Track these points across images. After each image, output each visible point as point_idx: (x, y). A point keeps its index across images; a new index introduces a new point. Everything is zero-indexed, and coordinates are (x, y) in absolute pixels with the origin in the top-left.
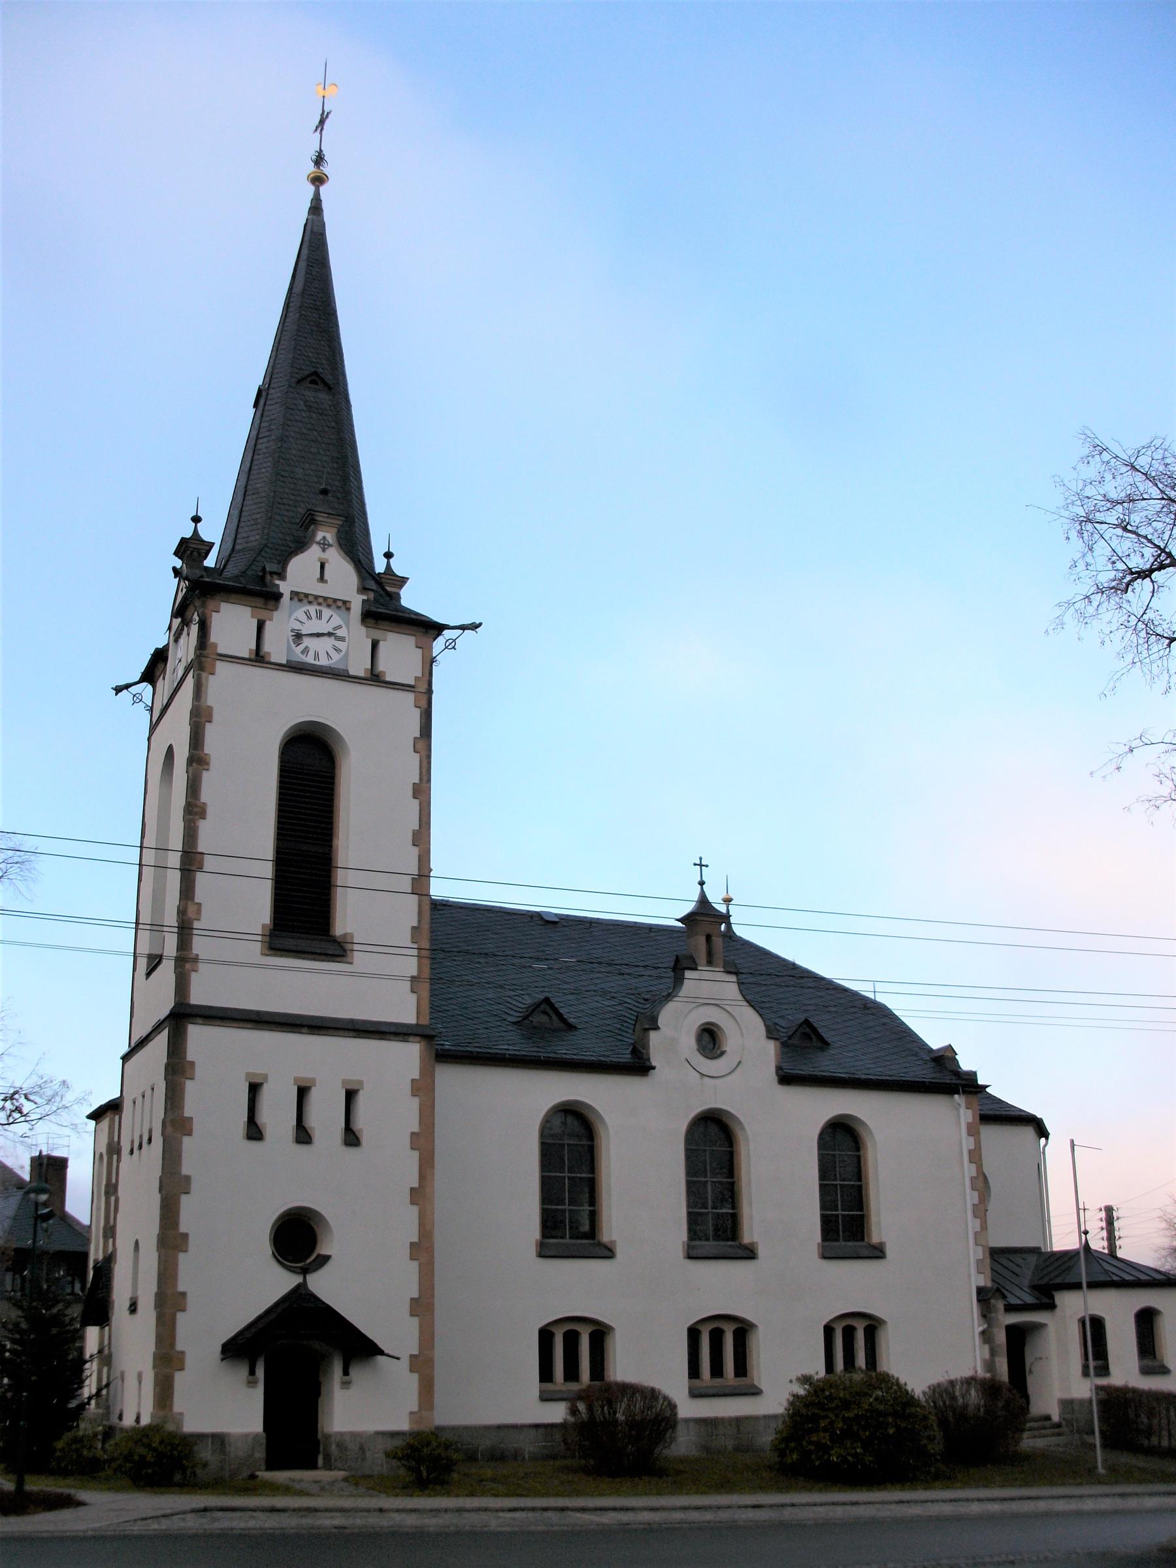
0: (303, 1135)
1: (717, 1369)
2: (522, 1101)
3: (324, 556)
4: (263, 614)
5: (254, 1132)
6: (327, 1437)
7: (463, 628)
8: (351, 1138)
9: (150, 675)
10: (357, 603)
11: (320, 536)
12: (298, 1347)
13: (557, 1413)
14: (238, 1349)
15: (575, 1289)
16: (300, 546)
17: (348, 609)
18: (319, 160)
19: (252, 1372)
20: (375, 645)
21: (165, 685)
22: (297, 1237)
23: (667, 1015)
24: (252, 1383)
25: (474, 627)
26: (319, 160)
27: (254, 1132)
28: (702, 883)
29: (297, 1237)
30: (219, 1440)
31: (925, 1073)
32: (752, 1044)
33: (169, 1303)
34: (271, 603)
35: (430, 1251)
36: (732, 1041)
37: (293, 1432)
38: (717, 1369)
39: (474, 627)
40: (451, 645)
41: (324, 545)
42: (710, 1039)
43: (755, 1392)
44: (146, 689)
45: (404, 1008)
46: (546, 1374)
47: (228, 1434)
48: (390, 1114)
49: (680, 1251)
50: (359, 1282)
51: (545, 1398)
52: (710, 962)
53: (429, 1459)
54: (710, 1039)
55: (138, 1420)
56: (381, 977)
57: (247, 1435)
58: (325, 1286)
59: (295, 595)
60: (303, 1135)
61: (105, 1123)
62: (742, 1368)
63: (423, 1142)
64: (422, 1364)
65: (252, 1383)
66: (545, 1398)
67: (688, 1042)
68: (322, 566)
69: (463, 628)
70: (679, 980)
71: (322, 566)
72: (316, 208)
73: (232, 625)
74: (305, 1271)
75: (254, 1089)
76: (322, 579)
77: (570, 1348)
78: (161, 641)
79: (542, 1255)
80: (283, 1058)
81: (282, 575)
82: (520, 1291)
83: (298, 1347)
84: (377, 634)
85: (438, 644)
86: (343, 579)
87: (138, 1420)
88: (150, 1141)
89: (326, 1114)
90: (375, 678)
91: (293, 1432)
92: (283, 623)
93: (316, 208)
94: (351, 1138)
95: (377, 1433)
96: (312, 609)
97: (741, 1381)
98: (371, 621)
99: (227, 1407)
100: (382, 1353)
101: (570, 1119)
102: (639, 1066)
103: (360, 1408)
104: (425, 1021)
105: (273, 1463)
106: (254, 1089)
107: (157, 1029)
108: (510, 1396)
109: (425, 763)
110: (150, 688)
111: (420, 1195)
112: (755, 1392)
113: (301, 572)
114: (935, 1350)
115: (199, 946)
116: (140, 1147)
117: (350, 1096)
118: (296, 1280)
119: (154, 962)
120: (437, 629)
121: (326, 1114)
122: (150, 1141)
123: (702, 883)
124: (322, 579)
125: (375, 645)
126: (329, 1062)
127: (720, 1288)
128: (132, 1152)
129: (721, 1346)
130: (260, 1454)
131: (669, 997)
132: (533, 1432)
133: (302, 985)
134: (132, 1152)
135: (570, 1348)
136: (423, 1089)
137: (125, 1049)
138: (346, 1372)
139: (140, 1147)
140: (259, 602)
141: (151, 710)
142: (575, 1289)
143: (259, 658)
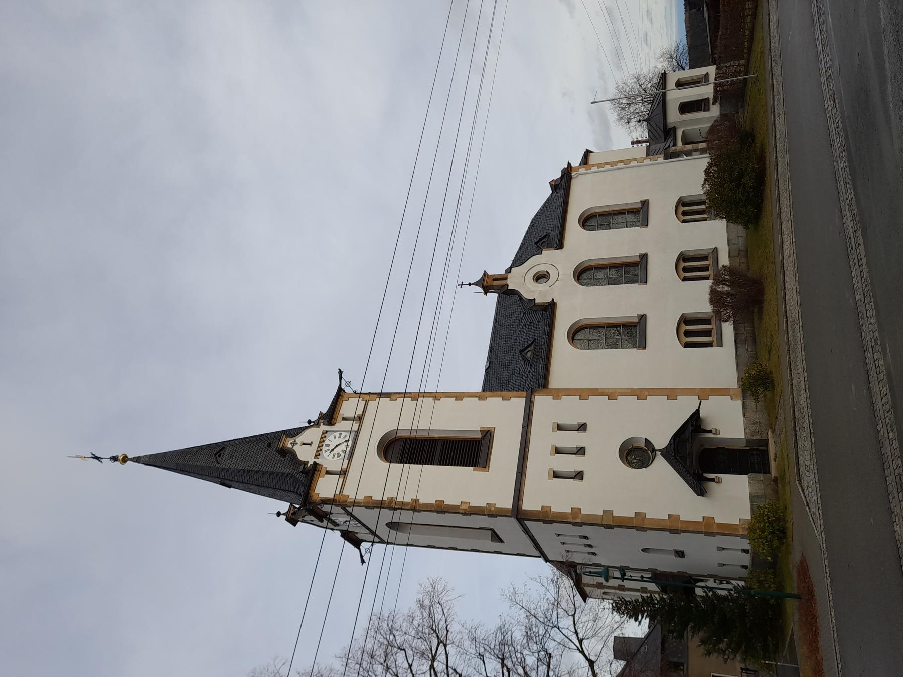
0: (581, 451)
1: (708, 333)
2: (568, 362)
3: (299, 444)
4: (323, 472)
5: (579, 476)
6: (748, 441)
7: (341, 378)
8: (583, 427)
9: (357, 543)
10: (323, 428)
11: (290, 446)
12: (696, 455)
13: (728, 329)
14: (699, 486)
15: (662, 331)
16: (293, 455)
17: (327, 432)
18: (114, 459)
19: (713, 480)
20: (328, 473)
21: (362, 533)
22: (636, 454)
23: (527, 295)
24: (719, 481)
25: (340, 372)
26: (114, 459)
27: (579, 476)
28: (470, 284)
29: (636, 454)
30: (753, 498)
31: (561, 193)
32: (545, 259)
33: (674, 526)
34: (318, 467)
35: (642, 390)
36: (543, 268)
37: (745, 459)
38: (708, 333)
39: (340, 372)
40: (348, 384)
41: (294, 444)
42: (541, 277)
43: (716, 251)
44: (364, 545)
45: (518, 403)
46: (709, 344)
47: (750, 494)
48: (570, 410)
49: (643, 287)
50: (660, 425)
51: (721, 344)
52: (506, 279)
53: (757, 384)
54: (541, 277)
55: (746, 551)
56: (502, 415)
57: (750, 483)
58: (661, 441)
59: (316, 456)
60: (581, 451)
61: (588, 590)
62: (705, 258)
63: (584, 394)
64: (704, 394)
65: (719, 481)
66: (721, 344)
67: (542, 287)
68: (304, 444)
69: (341, 378)
70: (514, 292)
71: (304, 444)
72: (137, 460)
73: (325, 488)
74: (654, 450)
75: (556, 475)
76: (310, 444)
77: (694, 332)
78: (339, 533)
79: (645, 348)
80: (541, 461)
81: (306, 463)
82: (663, 358)
83: (696, 455)
84: (340, 418)
85: (348, 390)
86: (312, 435)
87: (746, 551)
88: (586, 537)
89: (571, 440)
90: (360, 418)
91: (745, 459)
92: (329, 461)
93: (137, 460)
94: (583, 427)
95: (744, 416)
96: (324, 449)
97: (711, 256)
98: (333, 421)
99: (733, 498)
100: (698, 411)
101: (577, 337)
102: (550, 308)
103: (729, 422)
104: (524, 393)
105: (766, 470)
106: (556, 475)
107: (526, 531)
108: (720, 363)
109: (620, 219)
110: (363, 544)
111: (612, 395)
112: (716, 251)
113: (305, 455)
114: (690, 175)
115: (413, 388)
116: (590, 546)
117: (560, 428)
118: (658, 453)
119: (496, 537)
120: (340, 390)
121: (571, 440)
122: (586, 537)
123: (470, 284)
124: (310, 444)
125: (328, 473)
126: (543, 438)
127: (661, 268)
128: (594, 554)
129: (690, 265)
130: (761, 477)
131: (521, 297)
132: (739, 349)
133: (504, 453)
134: (594, 554)
135: (694, 332)
136: (558, 394)
137: (541, 560)
138: (710, 432)
139: (590, 546)
140: (317, 473)
141: (373, 542)
142: (662, 331)
143: (343, 473)
